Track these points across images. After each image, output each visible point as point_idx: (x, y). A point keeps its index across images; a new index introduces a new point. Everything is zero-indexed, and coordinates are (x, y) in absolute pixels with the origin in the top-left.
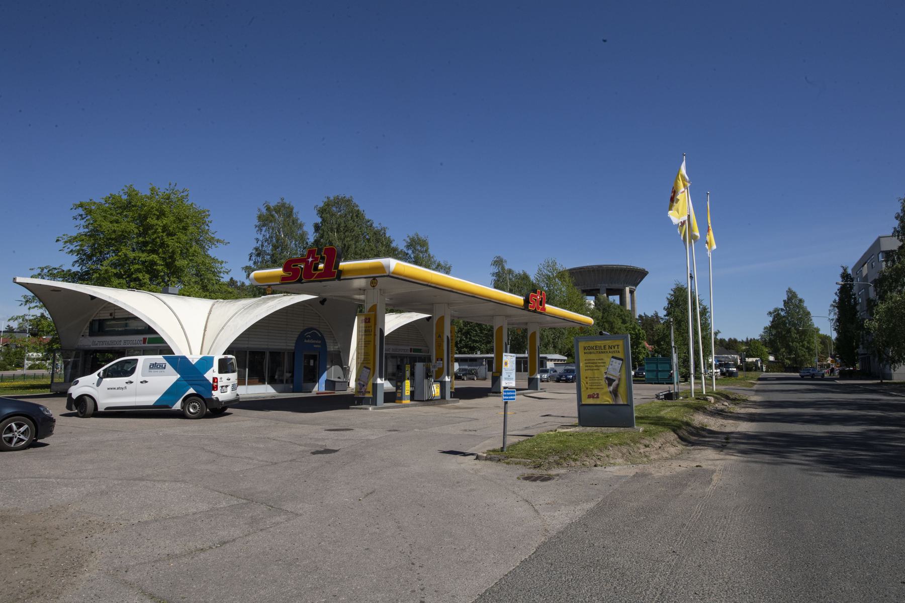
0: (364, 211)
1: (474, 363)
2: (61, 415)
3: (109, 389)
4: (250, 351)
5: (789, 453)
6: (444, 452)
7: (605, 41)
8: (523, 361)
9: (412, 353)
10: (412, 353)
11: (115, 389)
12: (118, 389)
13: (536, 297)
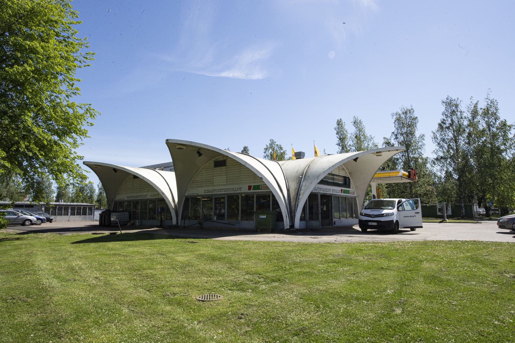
0: (403, 106)
1: (31, 209)
2: (497, 233)
3: (404, 217)
4: (191, 198)
5: (24, 232)
6: (73, 243)
7: (344, 23)
8: (77, 207)
9: (343, 194)
10: (343, 194)
11: (408, 217)
12: (410, 217)
13: (413, 172)
